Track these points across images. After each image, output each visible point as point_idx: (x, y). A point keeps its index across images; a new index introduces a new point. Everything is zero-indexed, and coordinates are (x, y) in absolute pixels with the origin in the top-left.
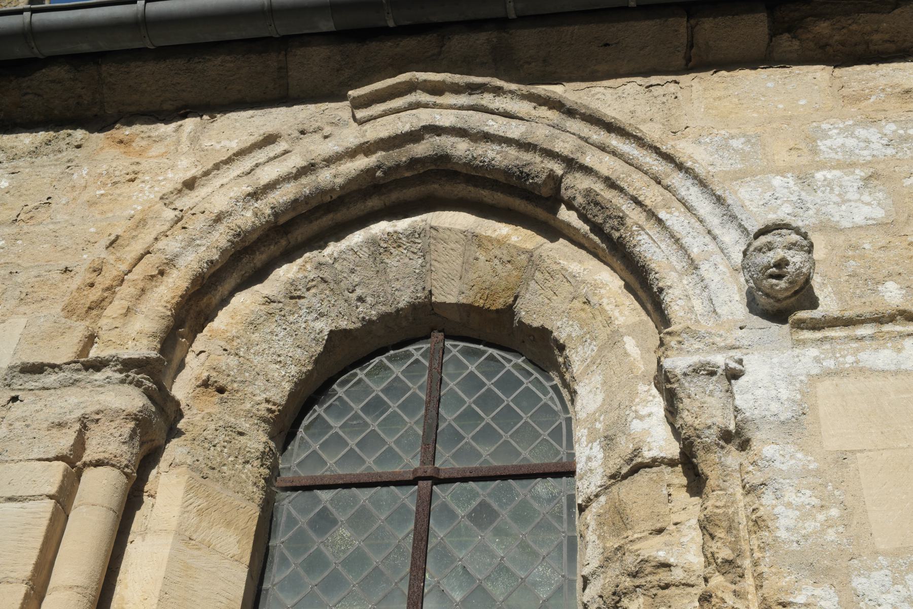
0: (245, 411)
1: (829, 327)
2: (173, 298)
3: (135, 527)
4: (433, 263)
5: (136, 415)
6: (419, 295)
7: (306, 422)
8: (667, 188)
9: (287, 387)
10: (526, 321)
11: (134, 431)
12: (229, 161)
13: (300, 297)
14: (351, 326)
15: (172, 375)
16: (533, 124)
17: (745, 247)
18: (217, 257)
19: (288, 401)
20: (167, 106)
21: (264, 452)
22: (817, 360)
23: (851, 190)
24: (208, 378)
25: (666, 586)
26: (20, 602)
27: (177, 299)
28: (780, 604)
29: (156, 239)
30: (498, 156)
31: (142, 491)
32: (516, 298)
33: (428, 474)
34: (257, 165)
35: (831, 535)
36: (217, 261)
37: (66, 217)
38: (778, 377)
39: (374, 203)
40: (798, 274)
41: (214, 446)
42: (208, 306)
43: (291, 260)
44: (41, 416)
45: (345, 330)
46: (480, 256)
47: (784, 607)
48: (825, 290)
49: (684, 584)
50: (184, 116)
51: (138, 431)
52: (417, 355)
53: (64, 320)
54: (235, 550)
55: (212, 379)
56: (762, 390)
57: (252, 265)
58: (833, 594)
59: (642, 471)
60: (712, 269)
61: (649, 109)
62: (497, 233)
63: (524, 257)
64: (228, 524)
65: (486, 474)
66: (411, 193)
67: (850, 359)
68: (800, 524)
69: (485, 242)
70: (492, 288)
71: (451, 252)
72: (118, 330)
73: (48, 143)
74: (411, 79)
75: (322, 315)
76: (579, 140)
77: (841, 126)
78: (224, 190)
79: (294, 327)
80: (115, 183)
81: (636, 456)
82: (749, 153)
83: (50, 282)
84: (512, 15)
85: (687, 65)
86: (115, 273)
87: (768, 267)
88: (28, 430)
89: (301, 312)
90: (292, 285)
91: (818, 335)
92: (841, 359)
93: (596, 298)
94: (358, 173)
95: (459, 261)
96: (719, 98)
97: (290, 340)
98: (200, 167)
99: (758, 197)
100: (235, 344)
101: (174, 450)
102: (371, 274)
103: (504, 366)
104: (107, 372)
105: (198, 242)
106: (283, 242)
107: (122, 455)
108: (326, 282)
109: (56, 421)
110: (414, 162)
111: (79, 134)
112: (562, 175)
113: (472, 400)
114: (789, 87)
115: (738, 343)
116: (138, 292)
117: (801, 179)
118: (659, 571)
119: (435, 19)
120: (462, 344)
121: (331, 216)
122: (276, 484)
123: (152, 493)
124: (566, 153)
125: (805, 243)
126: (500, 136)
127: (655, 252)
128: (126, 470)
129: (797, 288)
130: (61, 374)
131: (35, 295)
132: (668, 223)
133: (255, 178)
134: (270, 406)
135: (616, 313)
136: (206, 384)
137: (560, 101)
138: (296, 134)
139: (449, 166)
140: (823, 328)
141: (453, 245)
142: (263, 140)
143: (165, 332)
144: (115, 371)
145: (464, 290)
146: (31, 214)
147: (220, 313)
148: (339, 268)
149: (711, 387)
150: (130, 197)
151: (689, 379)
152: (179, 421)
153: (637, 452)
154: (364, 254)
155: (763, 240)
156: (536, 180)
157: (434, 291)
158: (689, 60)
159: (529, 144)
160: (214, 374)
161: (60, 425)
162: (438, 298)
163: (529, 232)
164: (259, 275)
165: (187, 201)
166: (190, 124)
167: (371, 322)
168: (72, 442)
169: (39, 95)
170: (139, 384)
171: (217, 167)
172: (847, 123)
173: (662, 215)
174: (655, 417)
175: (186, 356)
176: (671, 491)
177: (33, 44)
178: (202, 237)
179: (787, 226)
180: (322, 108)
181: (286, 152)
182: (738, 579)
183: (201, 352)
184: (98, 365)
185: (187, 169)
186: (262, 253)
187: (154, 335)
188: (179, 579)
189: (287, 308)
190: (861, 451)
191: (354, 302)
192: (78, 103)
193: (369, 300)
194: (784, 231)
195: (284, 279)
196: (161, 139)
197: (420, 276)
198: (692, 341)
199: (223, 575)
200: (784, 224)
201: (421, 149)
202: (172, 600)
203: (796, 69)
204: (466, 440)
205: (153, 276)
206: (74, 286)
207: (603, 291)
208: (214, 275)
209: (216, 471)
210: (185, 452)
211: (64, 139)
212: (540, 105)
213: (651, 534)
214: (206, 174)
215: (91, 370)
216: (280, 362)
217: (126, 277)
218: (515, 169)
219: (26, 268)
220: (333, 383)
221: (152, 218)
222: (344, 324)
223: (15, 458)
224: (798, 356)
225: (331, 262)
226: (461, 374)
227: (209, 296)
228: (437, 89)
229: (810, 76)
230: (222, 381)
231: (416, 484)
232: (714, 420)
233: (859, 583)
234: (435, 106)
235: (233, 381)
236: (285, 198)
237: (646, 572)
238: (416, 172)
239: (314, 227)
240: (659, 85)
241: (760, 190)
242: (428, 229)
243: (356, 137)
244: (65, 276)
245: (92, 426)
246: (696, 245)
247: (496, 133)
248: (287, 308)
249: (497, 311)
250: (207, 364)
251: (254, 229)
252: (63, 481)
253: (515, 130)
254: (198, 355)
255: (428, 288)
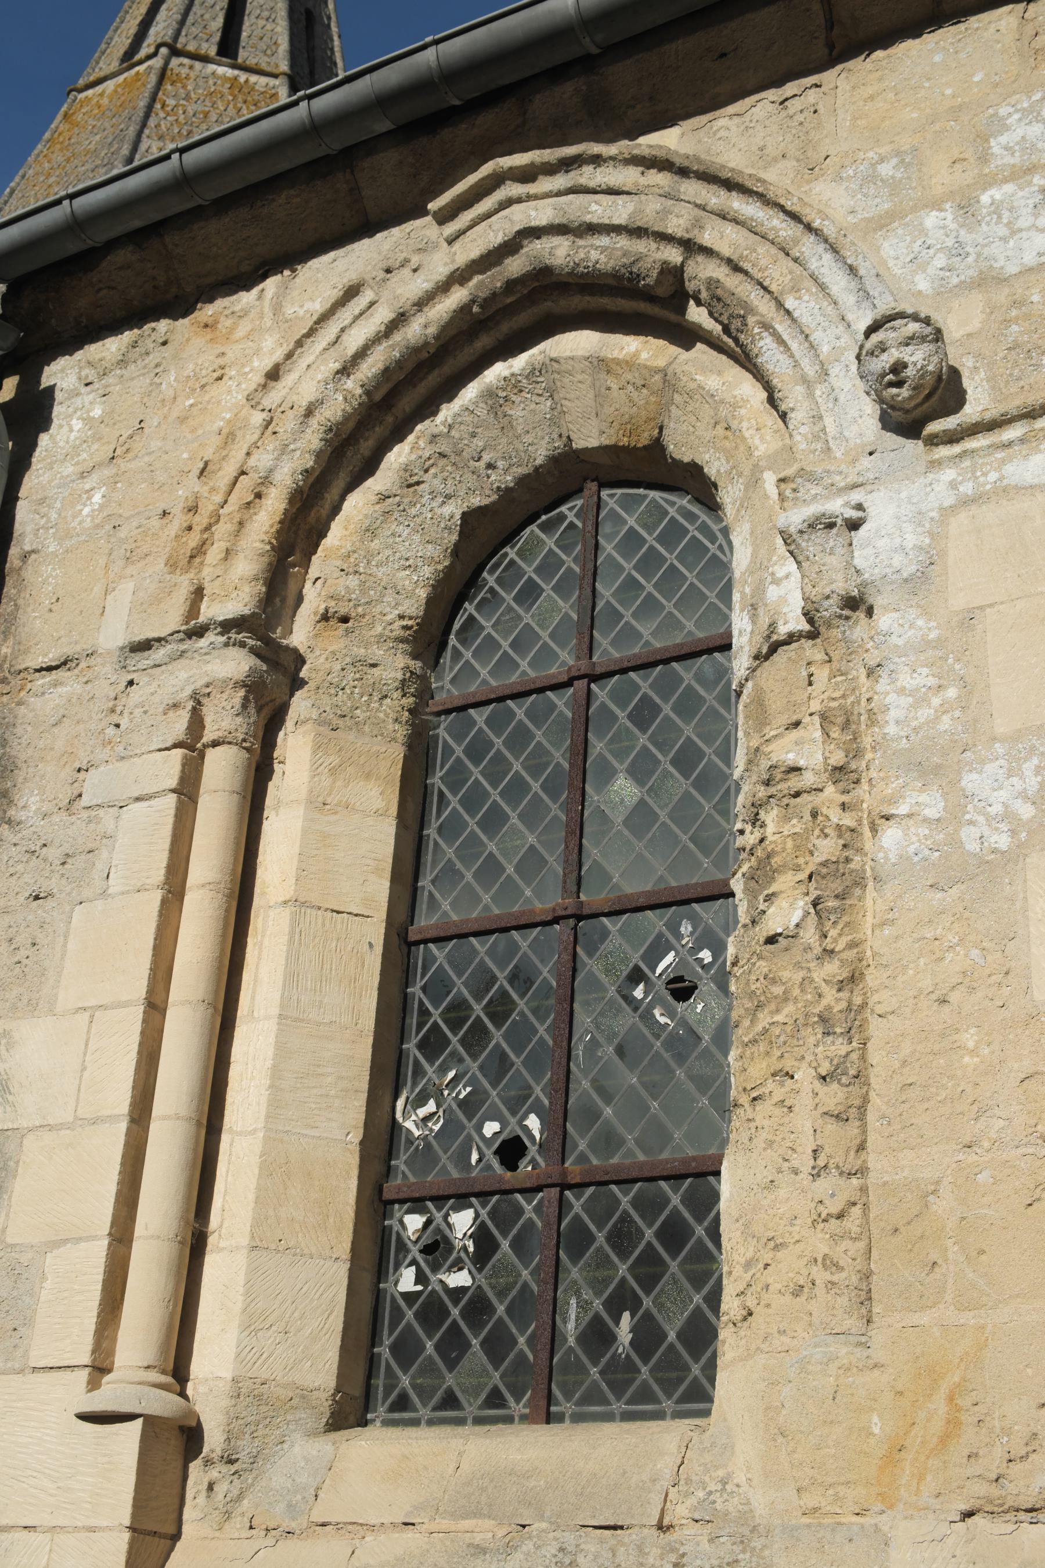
0: (376, 636)
1: (969, 435)
2: (272, 526)
3: (269, 801)
4: (564, 402)
5: (243, 681)
6: (556, 445)
7: (457, 626)
8: (796, 260)
9: (423, 593)
10: (677, 456)
11: (246, 699)
12: (311, 332)
13: (418, 483)
14: (486, 501)
15: (290, 613)
16: (643, 197)
17: (857, 351)
18: (311, 463)
19: (426, 610)
20: (245, 267)
21: (404, 679)
22: (953, 485)
23: (1024, 211)
24: (327, 610)
25: (797, 795)
26: (157, 909)
27: (277, 527)
28: (883, 817)
29: (248, 454)
30: (602, 256)
31: (272, 759)
32: (661, 428)
33: (582, 672)
34: (343, 330)
35: (946, 723)
36: (313, 468)
37: (159, 444)
38: (905, 518)
39: (484, 342)
40: (922, 375)
41: (343, 689)
42: (318, 520)
43: (401, 439)
44: (157, 699)
45: (480, 507)
46: (612, 385)
47: (887, 819)
48: (976, 378)
49: (815, 790)
50: (264, 277)
51: (251, 697)
52: (571, 517)
53: (168, 577)
54: (378, 803)
55: (331, 610)
56: (884, 540)
57: (359, 456)
58: (939, 799)
59: (780, 650)
60: (842, 374)
61: (781, 139)
62: (624, 352)
63: (657, 377)
64: (368, 776)
65: (646, 661)
66: (523, 319)
67: (993, 476)
68: (912, 714)
69: (614, 366)
70: (633, 421)
71: (579, 385)
72: (220, 579)
73: (134, 345)
74: (494, 170)
75: (448, 497)
76: (696, 209)
77: (1025, 105)
78: (311, 371)
79: (418, 520)
80: (203, 387)
81: (772, 632)
82: (900, 181)
83: (150, 532)
84: (595, 51)
85: (830, 54)
86: (211, 508)
87: (883, 375)
88: (145, 717)
89: (424, 500)
90: (406, 470)
91: (957, 449)
92: (982, 479)
93: (736, 422)
94: (450, 315)
95: (591, 395)
96: (872, 98)
97: (417, 538)
98: (285, 345)
99: (905, 251)
100: (352, 560)
101: (300, 705)
102: (496, 432)
103: (667, 513)
104: (211, 637)
105: (292, 447)
106: (390, 419)
107: (237, 730)
108: (445, 456)
109: (171, 702)
110: (511, 285)
111: (163, 325)
112: (683, 264)
113: (631, 565)
114: (963, 55)
115: (861, 479)
116: (235, 527)
117: (963, 207)
118: (790, 776)
119: (506, 81)
120: (619, 492)
121: (436, 373)
122: (428, 710)
123: (281, 759)
124: (679, 233)
125: (929, 330)
126: (606, 225)
127: (778, 361)
128: (244, 744)
129: (927, 392)
130: (169, 647)
131: (139, 550)
132: (796, 315)
133: (342, 347)
134: (405, 623)
135: (757, 442)
136: (325, 617)
137: (667, 160)
138: (382, 275)
139: (554, 279)
140: (963, 439)
141: (580, 377)
142: (344, 295)
143: (268, 571)
144: (217, 634)
145: (604, 429)
146: (127, 446)
147: (333, 525)
148: (457, 436)
149: (831, 543)
150: (219, 402)
151: (806, 536)
152: (300, 670)
153: (772, 627)
154: (482, 411)
155: (875, 338)
156: (648, 280)
157: (573, 436)
158: (831, 47)
159: (639, 229)
160: (332, 603)
161: (175, 706)
162: (579, 444)
163: (661, 343)
164: (369, 467)
165: (274, 397)
166: (271, 284)
167: (508, 490)
168: (185, 725)
169: (113, 288)
170: (242, 645)
171: (299, 344)
172: (1034, 98)
173: (790, 303)
174: (793, 579)
175: (303, 586)
176: (812, 669)
177: (83, 236)
178: (295, 440)
179: (901, 315)
180: (408, 230)
181: (372, 304)
182: (852, 786)
183: (317, 579)
184: (199, 632)
185: (272, 351)
186: (366, 440)
187: (256, 579)
188: (316, 852)
189: (406, 500)
190: (991, 606)
191: (483, 472)
192: (154, 287)
193: (500, 464)
194: (898, 322)
195: (396, 466)
196: (244, 314)
197: (553, 422)
198: (808, 485)
199: (367, 835)
200: (897, 314)
201: (515, 266)
202: (312, 876)
203: (974, 22)
204: (625, 619)
205: (248, 503)
206: (173, 534)
207: (743, 411)
208: (313, 485)
209: (347, 718)
210: (310, 705)
211: (149, 335)
212: (648, 168)
213: (787, 729)
214: (289, 356)
215: (194, 638)
216: (410, 566)
217: (221, 511)
218: (623, 270)
219: (128, 518)
220: (483, 571)
221: (240, 428)
222: (477, 501)
223: (138, 751)
224: (931, 484)
225: (446, 430)
226: (619, 532)
227: (316, 509)
228: (527, 175)
229: (992, 29)
230: (343, 611)
231: (572, 685)
232: (834, 587)
233: (970, 781)
234: (530, 198)
235: (356, 606)
236: (373, 370)
237: (777, 780)
238: (519, 295)
239: (421, 390)
240: (795, 95)
241: (908, 238)
242: (548, 362)
243: (446, 264)
244: (165, 521)
245: (205, 701)
246: (826, 340)
247: (600, 221)
248: (406, 500)
249: (645, 447)
250: (323, 594)
251: (347, 418)
252: (183, 771)
253: (620, 211)
254: (314, 583)
255: (565, 434)
